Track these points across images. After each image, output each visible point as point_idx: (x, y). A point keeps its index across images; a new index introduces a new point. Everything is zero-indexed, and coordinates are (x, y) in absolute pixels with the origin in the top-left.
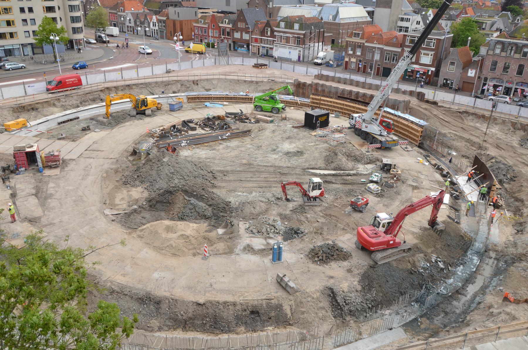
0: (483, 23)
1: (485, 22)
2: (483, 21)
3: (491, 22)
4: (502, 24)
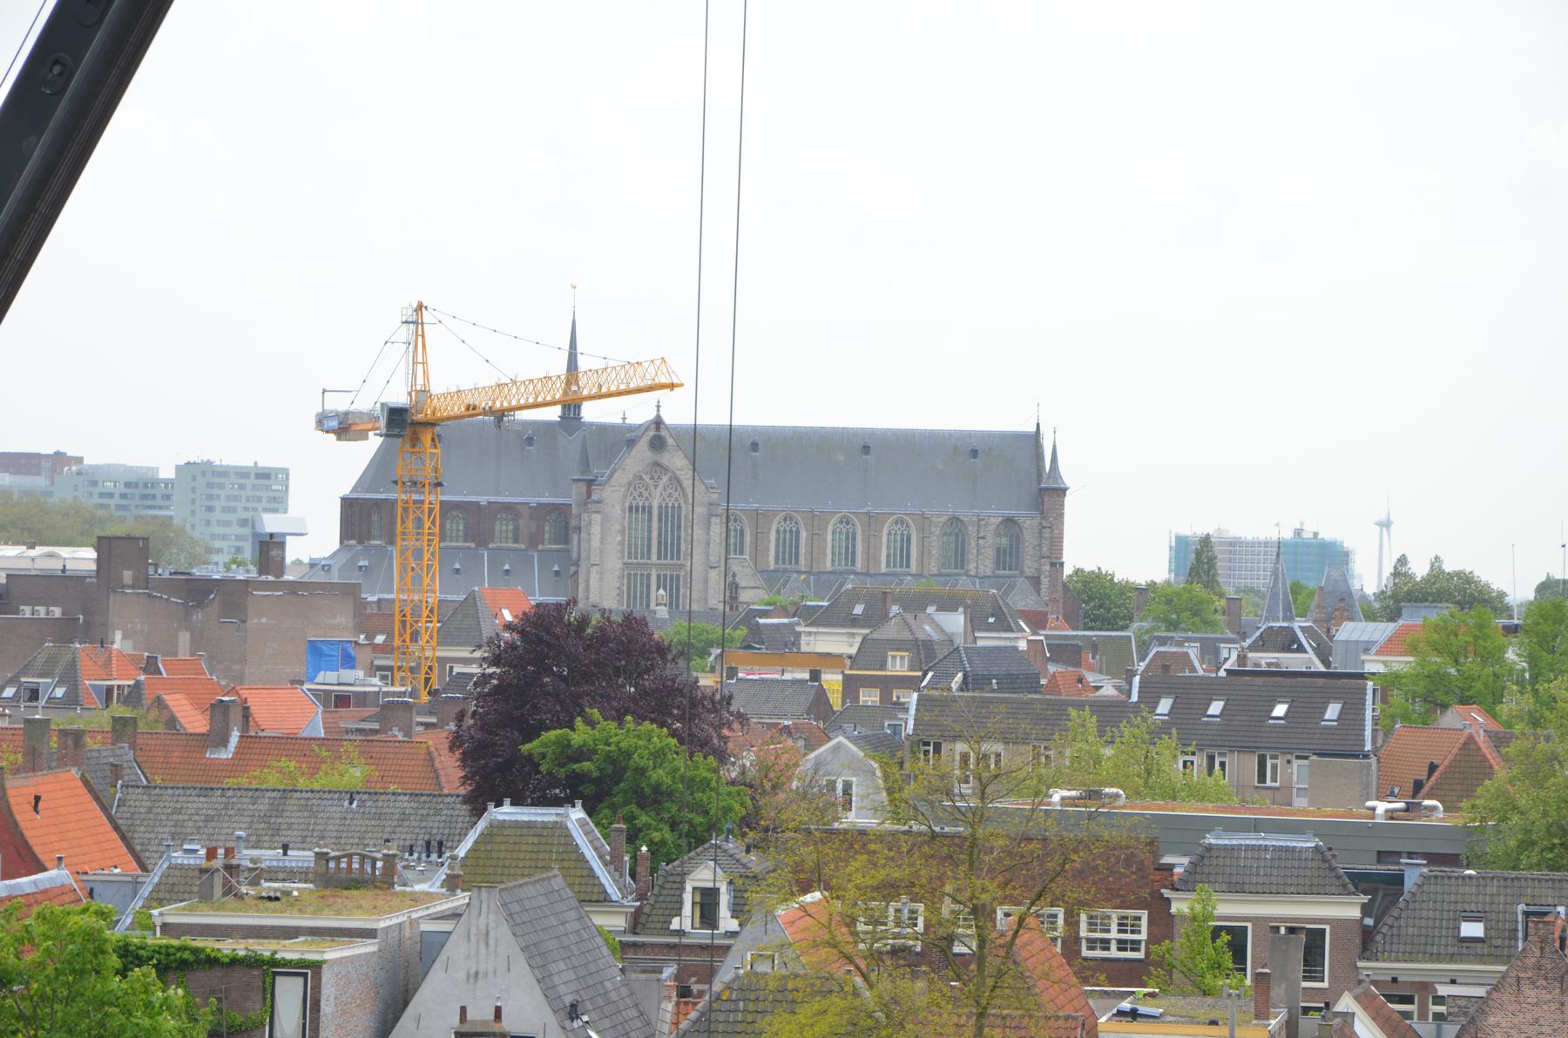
0: (271, 968)
1: (290, 951)
2: (265, 948)
3: (368, 947)
4: (521, 966)
